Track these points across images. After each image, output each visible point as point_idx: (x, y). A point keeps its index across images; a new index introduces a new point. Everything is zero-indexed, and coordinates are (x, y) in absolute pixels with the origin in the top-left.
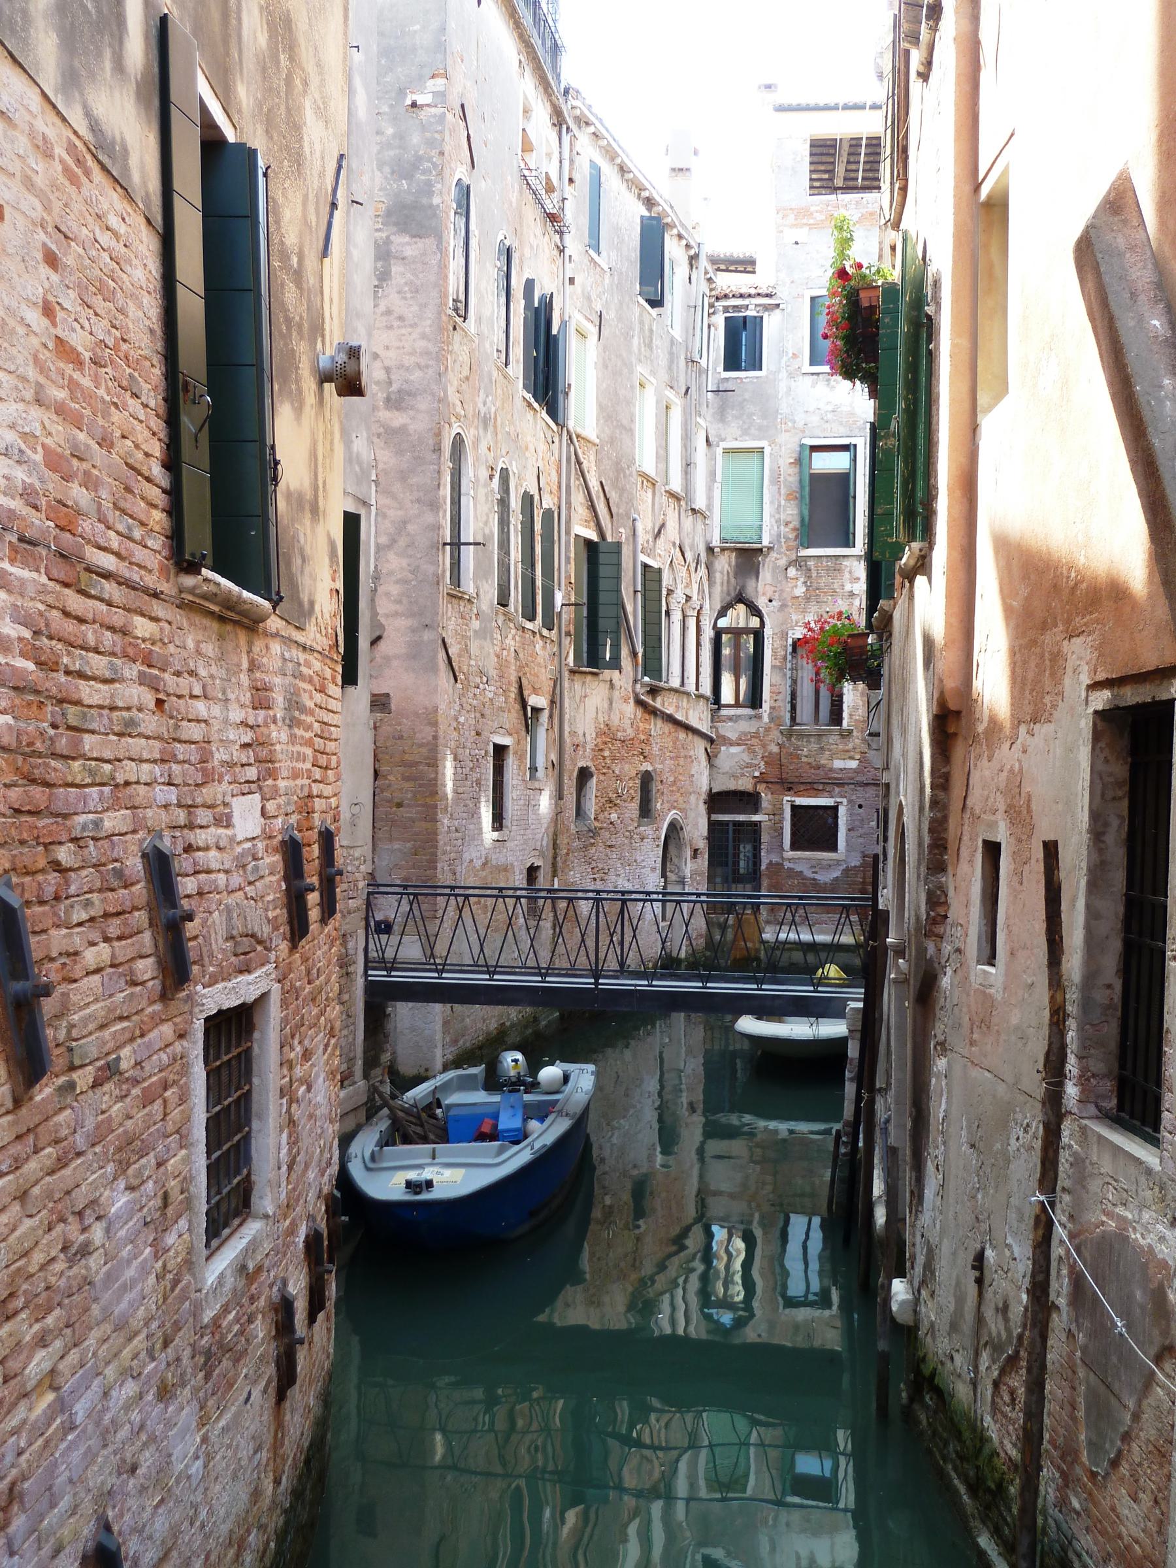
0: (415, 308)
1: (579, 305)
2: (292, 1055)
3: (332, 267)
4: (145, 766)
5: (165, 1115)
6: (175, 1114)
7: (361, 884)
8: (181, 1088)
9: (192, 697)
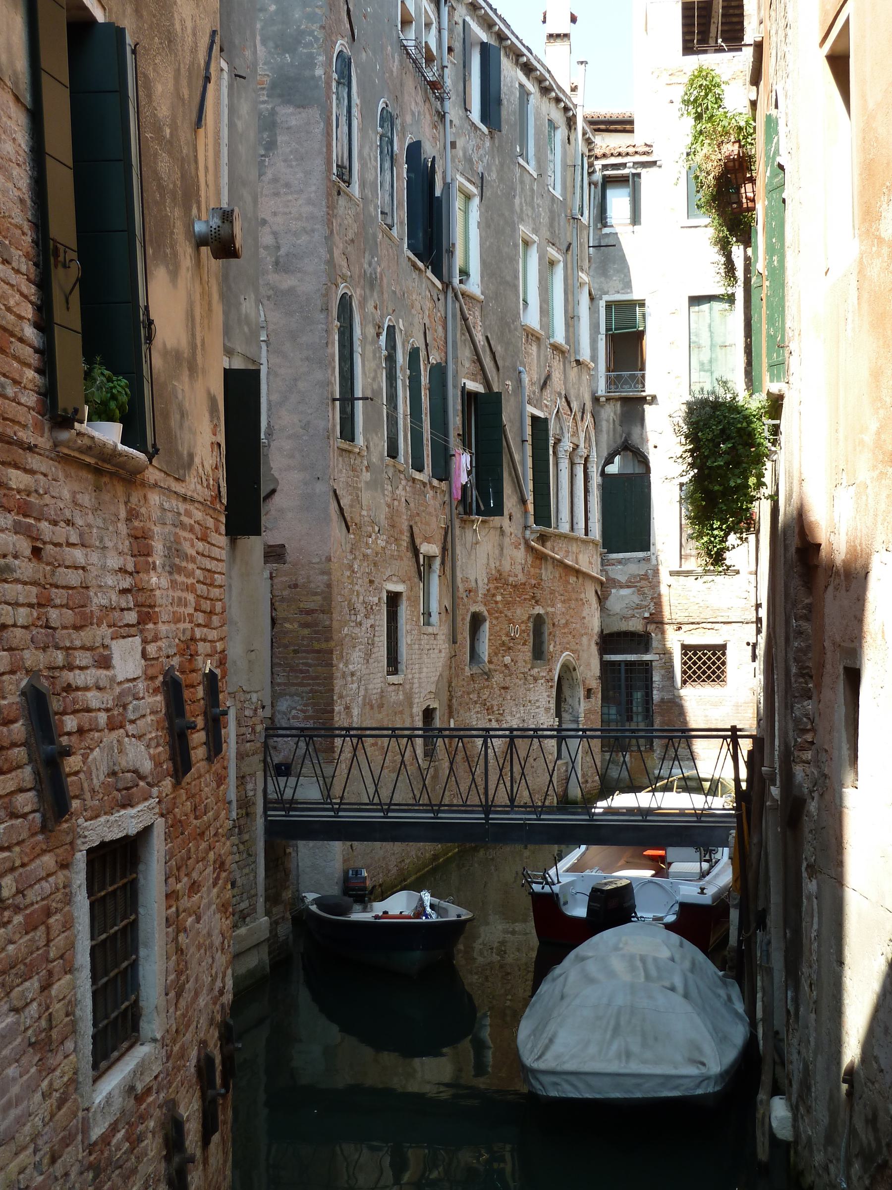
0: (300, 175)
1: (460, 167)
2: (179, 886)
3: (206, 137)
4: (22, 610)
5: (49, 941)
6: (60, 941)
7: (259, 728)
8: (65, 916)
9: (69, 545)
